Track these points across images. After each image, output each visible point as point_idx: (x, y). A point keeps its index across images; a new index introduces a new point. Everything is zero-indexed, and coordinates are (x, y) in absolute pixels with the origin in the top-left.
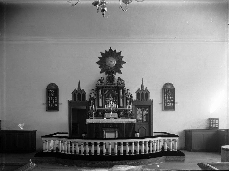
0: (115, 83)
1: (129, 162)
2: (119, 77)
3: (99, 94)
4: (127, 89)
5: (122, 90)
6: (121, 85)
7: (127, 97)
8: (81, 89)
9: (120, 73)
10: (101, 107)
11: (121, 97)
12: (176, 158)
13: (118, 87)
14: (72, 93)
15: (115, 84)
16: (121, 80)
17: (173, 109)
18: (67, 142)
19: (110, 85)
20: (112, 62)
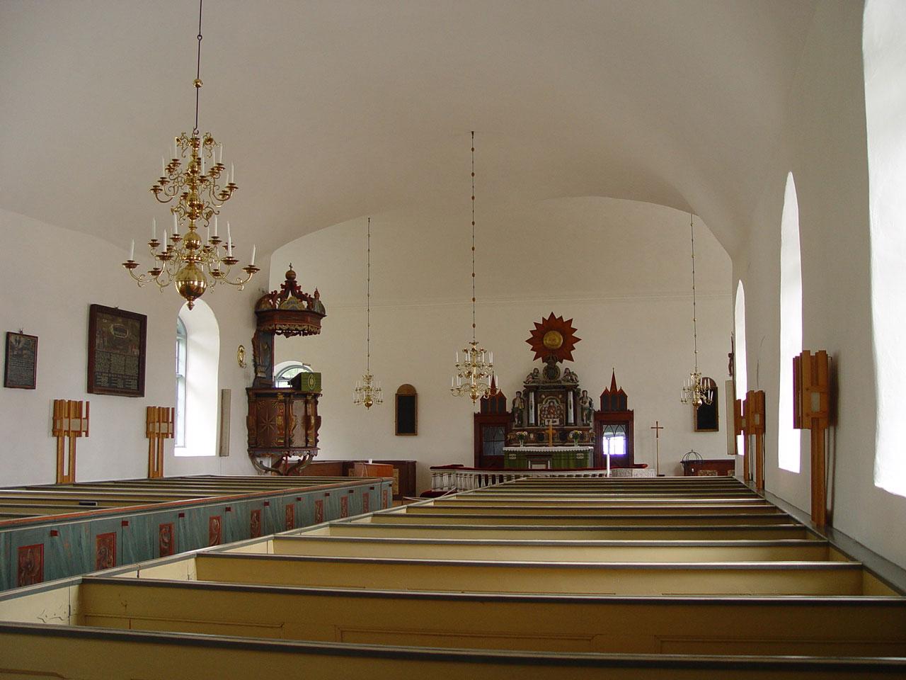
0: (560, 379)
11: (532, 407)
18: (473, 476)
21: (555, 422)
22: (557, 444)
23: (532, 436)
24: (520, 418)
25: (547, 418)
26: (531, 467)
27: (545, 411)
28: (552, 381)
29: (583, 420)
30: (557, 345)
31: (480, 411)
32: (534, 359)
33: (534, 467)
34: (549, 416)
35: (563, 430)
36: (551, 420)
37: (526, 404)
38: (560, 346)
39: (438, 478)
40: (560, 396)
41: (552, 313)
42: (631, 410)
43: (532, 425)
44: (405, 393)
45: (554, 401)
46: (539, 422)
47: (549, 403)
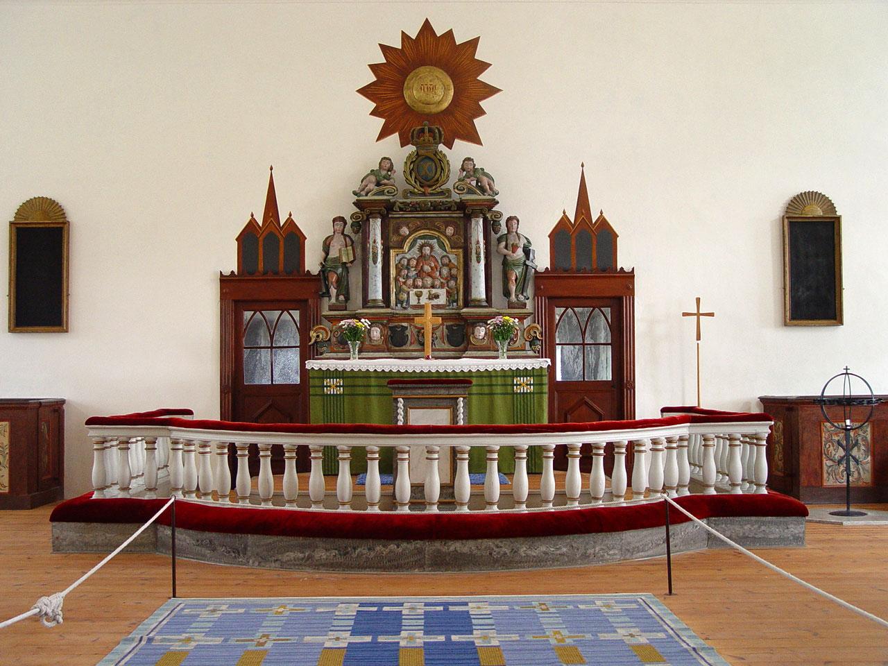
0: (449, 185)
3: (371, 241)
5: (481, 220)
6: (475, 193)
8: (283, 220)
9: (473, 137)
12: (763, 528)
13: (462, 206)
15: (448, 191)
16: (475, 170)
19: (424, 194)
20: (432, 89)
21: (437, 297)
22: (442, 354)
23: (376, 333)
26: (406, 417)
28: (430, 190)
29: (507, 293)
30: (440, 102)
32: (378, 140)
33: (419, 417)
35: (459, 317)
36: (425, 291)
37: (359, 251)
38: (446, 105)
39: (114, 454)
40: (450, 231)
41: (427, 22)
42: (627, 269)
43: (374, 304)
44: (36, 219)
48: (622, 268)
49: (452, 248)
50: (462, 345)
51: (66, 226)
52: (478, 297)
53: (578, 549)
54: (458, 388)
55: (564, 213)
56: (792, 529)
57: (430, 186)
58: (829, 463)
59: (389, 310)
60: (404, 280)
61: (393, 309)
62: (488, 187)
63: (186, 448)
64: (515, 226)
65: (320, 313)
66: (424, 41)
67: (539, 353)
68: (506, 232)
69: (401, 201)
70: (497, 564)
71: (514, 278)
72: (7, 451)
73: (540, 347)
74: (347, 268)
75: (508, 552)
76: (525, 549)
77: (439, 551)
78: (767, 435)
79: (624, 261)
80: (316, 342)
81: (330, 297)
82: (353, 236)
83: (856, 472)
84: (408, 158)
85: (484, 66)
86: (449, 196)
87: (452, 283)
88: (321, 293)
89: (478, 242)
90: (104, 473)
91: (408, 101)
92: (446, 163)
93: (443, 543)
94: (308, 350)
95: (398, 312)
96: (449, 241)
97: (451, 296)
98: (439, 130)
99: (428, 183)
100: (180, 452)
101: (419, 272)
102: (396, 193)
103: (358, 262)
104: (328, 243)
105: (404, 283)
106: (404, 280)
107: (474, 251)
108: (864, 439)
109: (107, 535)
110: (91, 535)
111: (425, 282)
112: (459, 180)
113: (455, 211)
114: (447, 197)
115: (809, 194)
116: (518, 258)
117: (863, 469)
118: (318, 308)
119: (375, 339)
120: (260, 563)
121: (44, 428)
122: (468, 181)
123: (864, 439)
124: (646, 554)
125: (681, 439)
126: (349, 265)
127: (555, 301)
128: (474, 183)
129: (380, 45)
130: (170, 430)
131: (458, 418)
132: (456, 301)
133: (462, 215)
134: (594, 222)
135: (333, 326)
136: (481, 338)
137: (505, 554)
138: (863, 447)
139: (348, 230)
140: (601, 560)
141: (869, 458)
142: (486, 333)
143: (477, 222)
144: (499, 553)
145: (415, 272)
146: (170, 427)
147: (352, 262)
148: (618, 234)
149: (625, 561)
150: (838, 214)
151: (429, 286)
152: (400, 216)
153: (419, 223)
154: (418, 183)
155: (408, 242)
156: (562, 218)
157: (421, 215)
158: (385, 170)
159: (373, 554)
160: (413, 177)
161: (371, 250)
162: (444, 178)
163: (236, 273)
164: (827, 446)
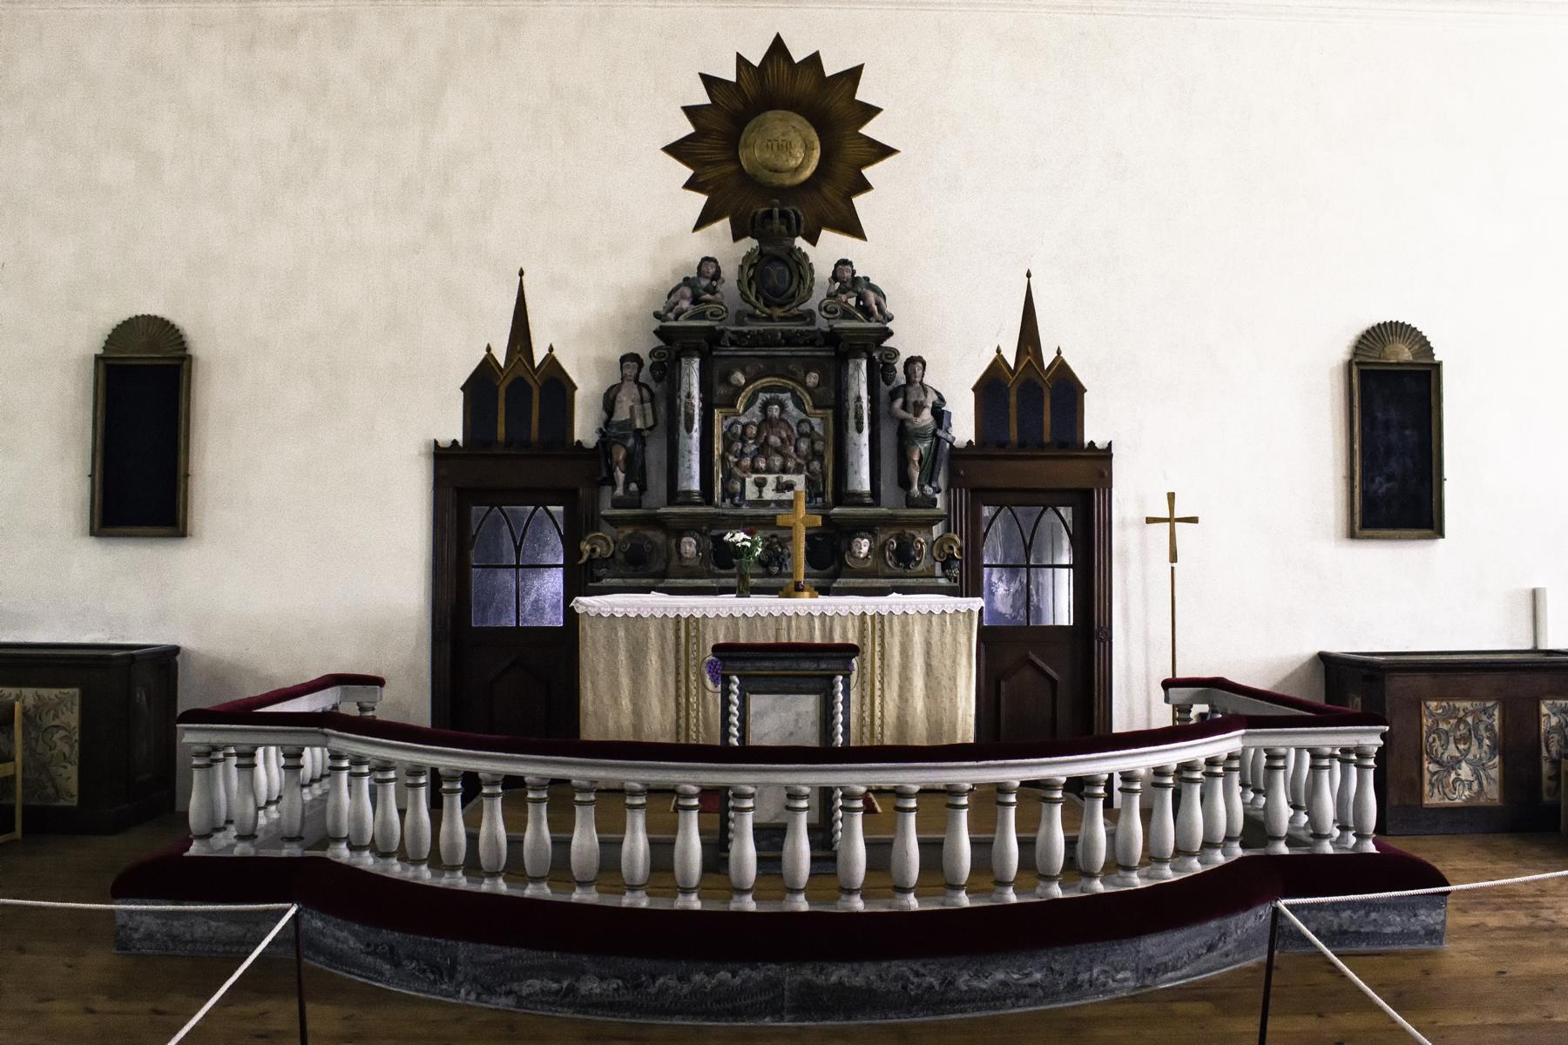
0: (813, 304)
1: (977, 976)
2: (844, 262)
3: (683, 395)
4: (903, 357)
7: (902, 422)
8: (539, 356)
9: (853, 228)
10: (697, 498)
12: (1373, 915)
13: (833, 337)
14: (950, 413)
15: (811, 313)
16: (855, 280)
17: (1430, 527)
19: (770, 318)
20: (786, 147)
24: (637, 470)
25: (755, 470)
27: (743, 438)
28: (779, 312)
29: (904, 482)
30: (798, 169)
31: (459, 436)
32: (698, 227)
34: (762, 464)
36: (771, 478)
37: (662, 409)
39: (229, 774)
40: (813, 379)
42: (1100, 443)
45: (786, 396)
46: (718, 488)
47: (765, 407)
48: (1092, 443)
49: (815, 407)
50: (832, 568)
51: (185, 363)
52: (859, 489)
53: (1062, 974)
54: (835, 658)
55: (998, 351)
56: (1424, 917)
57: (780, 306)
58: (1433, 767)
59: (711, 510)
60: (736, 460)
61: (717, 507)
62: (875, 308)
63: (354, 770)
64: (919, 372)
65: (598, 512)
66: (773, 70)
67: (955, 581)
68: (903, 382)
69: (733, 328)
70: (915, 1007)
71: (916, 458)
72: (76, 737)
73: (958, 572)
74: (643, 438)
75: (936, 984)
76: (967, 977)
77: (808, 985)
78: (1376, 749)
79: (1094, 432)
80: (590, 559)
81: (614, 485)
82: (652, 385)
83: (1476, 782)
84: (745, 259)
85: (870, 112)
86: (812, 323)
87: (816, 465)
88: (599, 479)
89: (859, 399)
90: (211, 804)
91: (745, 167)
92: (807, 267)
93: (818, 969)
94: (580, 580)
95: (726, 512)
96: (810, 395)
97: (813, 486)
98: (796, 214)
99: (777, 300)
100: (344, 775)
101: (762, 446)
102: (725, 315)
103: (661, 430)
104: (611, 396)
105: (737, 464)
106: (736, 460)
107: (852, 414)
108: (1489, 728)
109: (213, 923)
110: (181, 922)
111: (772, 463)
112: (829, 296)
113: (820, 346)
114: (808, 324)
115: (1391, 326)
116: (923, 425)
117: (1488, 777)
118: (595, 502)
119: (688, 556)
120: (479, 995)
121: (141, 696)
122: (844, 297)
123: (1489, 728)
124: (1179, 974)
125: (1231, 757)
126: (646, 433)
127: (981, 494)
128: (852, 301)
129: (700, 74)
130: (326, 735)
131: (835, 711)
132: (822, 495)
133: (833, 354)
134: (1046, 367)
135: (618, 533)
136: (862, 556)
137: (931, 987)
138: (1487, 742)
139: (645, 375)
140: (1102, 992)
141: (1497, 760)
142: (870, 550)
143: (858, 367)
144: (919, 986)
145: (754, 447)
146: (327, 730)
147: (651, 429)
148: (1086, 387)
149: (1144, 990)
150: (1437, 358)
151: (777, 469)
152: (731, 353)
153: (761, 366)
154: (762, 301)
155: (744, 397)
156: (995, 361)
157: (764, 353)
158: (707, 278)
159: (686, 988)
160: (754, 290)
161: (683, 409)
162: (804, 293)
163: (461, 444)
164: (1431, 739)
